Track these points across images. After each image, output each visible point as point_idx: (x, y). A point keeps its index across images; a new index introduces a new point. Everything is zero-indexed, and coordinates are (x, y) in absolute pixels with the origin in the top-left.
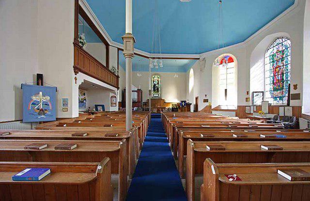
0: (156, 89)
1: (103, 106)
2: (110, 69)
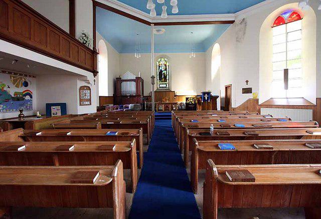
0: (163, 77)
1: (63, 107)
2: (77, 38)
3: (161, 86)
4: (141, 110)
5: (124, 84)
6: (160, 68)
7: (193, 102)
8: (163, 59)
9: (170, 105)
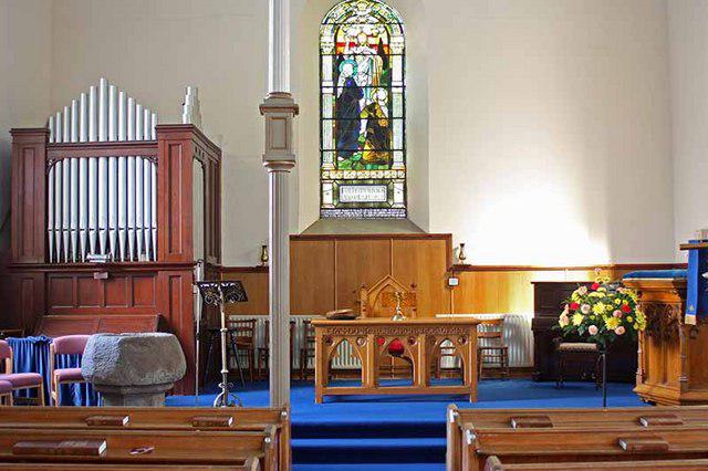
3: (349, 194)
4: (184, 386)
5: (67, 173)
6: (346, 69)
7: (612, 324)
8: (363, 9)
9: (420, 342)
